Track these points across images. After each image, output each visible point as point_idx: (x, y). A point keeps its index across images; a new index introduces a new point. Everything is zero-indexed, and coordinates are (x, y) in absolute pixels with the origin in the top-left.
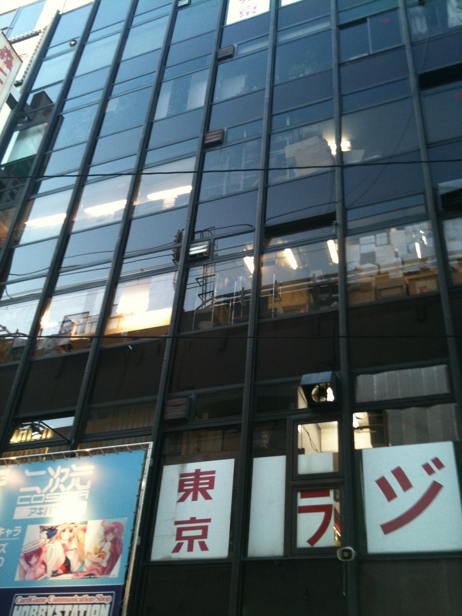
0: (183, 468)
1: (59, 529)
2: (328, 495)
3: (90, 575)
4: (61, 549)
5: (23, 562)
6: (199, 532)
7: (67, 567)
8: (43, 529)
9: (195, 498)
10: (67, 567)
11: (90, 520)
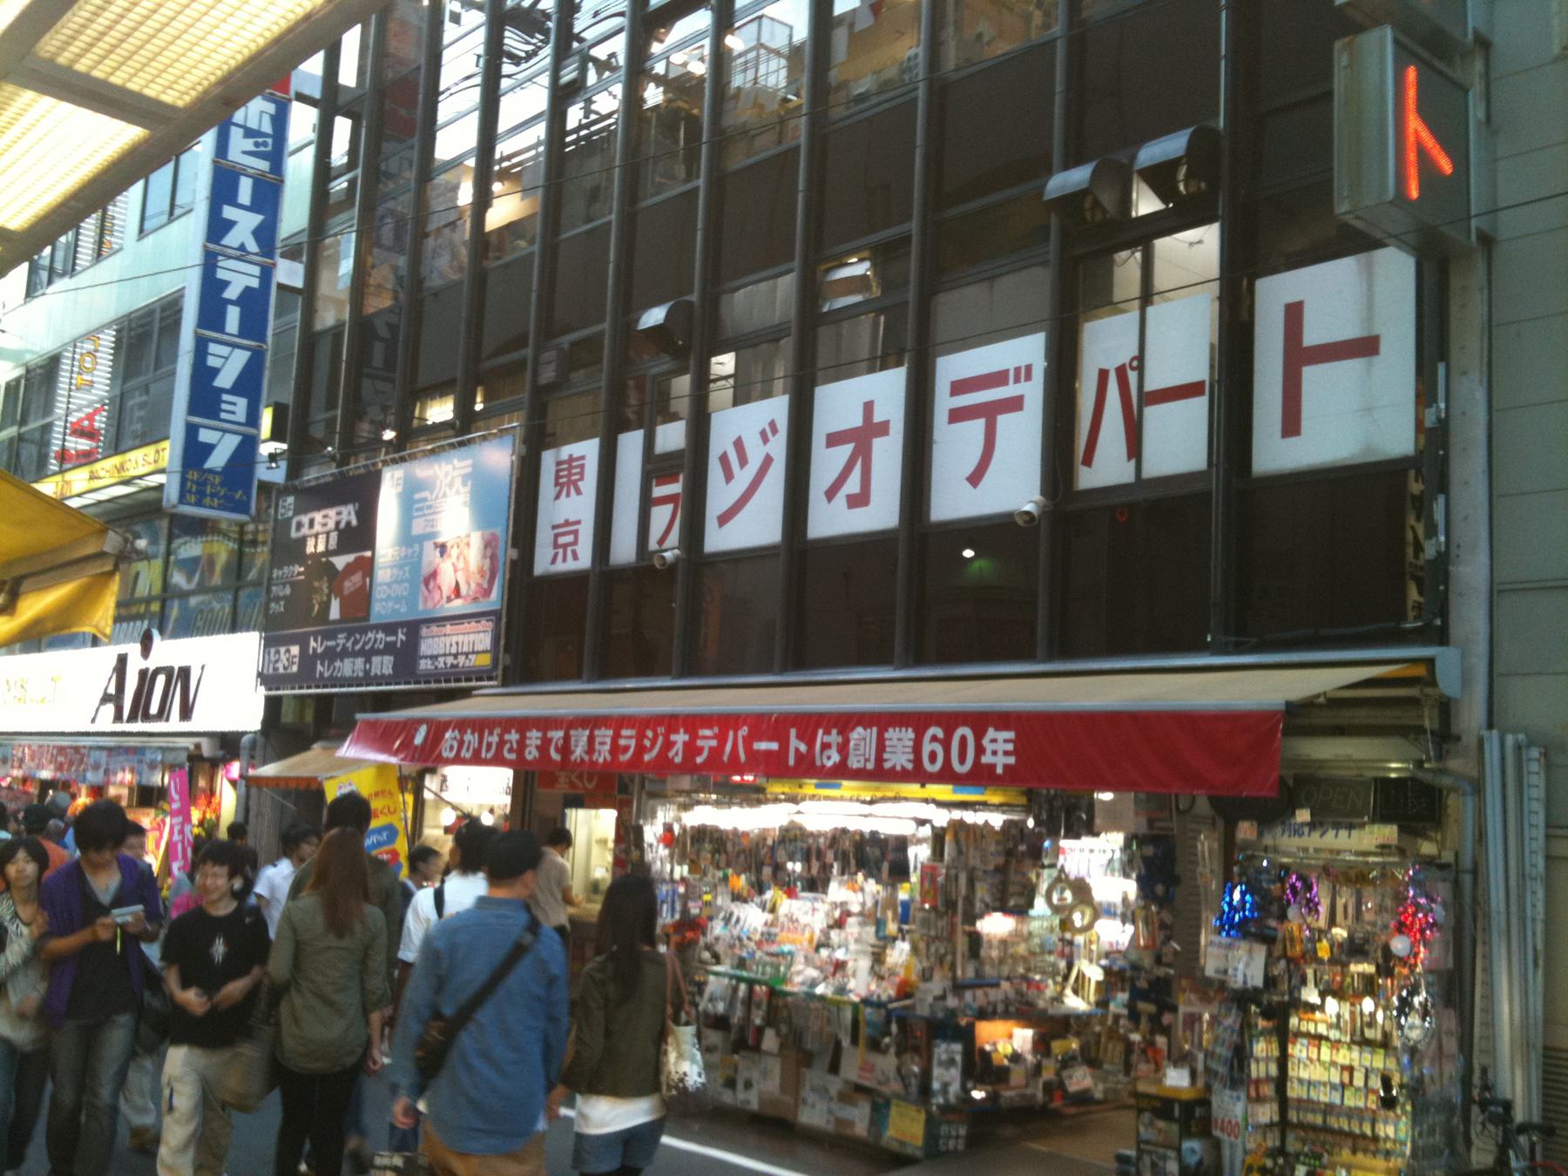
0: (558, 454)
1: (449, 545)
2: (676, 481)
3: (475, 599)
4: (451, 569)
5: (423, 587)
6: (570, 538)
7: (457, 592)
8: (436, 546)
9: (568, 495)
10: (457, 592)
11: (104, 543)
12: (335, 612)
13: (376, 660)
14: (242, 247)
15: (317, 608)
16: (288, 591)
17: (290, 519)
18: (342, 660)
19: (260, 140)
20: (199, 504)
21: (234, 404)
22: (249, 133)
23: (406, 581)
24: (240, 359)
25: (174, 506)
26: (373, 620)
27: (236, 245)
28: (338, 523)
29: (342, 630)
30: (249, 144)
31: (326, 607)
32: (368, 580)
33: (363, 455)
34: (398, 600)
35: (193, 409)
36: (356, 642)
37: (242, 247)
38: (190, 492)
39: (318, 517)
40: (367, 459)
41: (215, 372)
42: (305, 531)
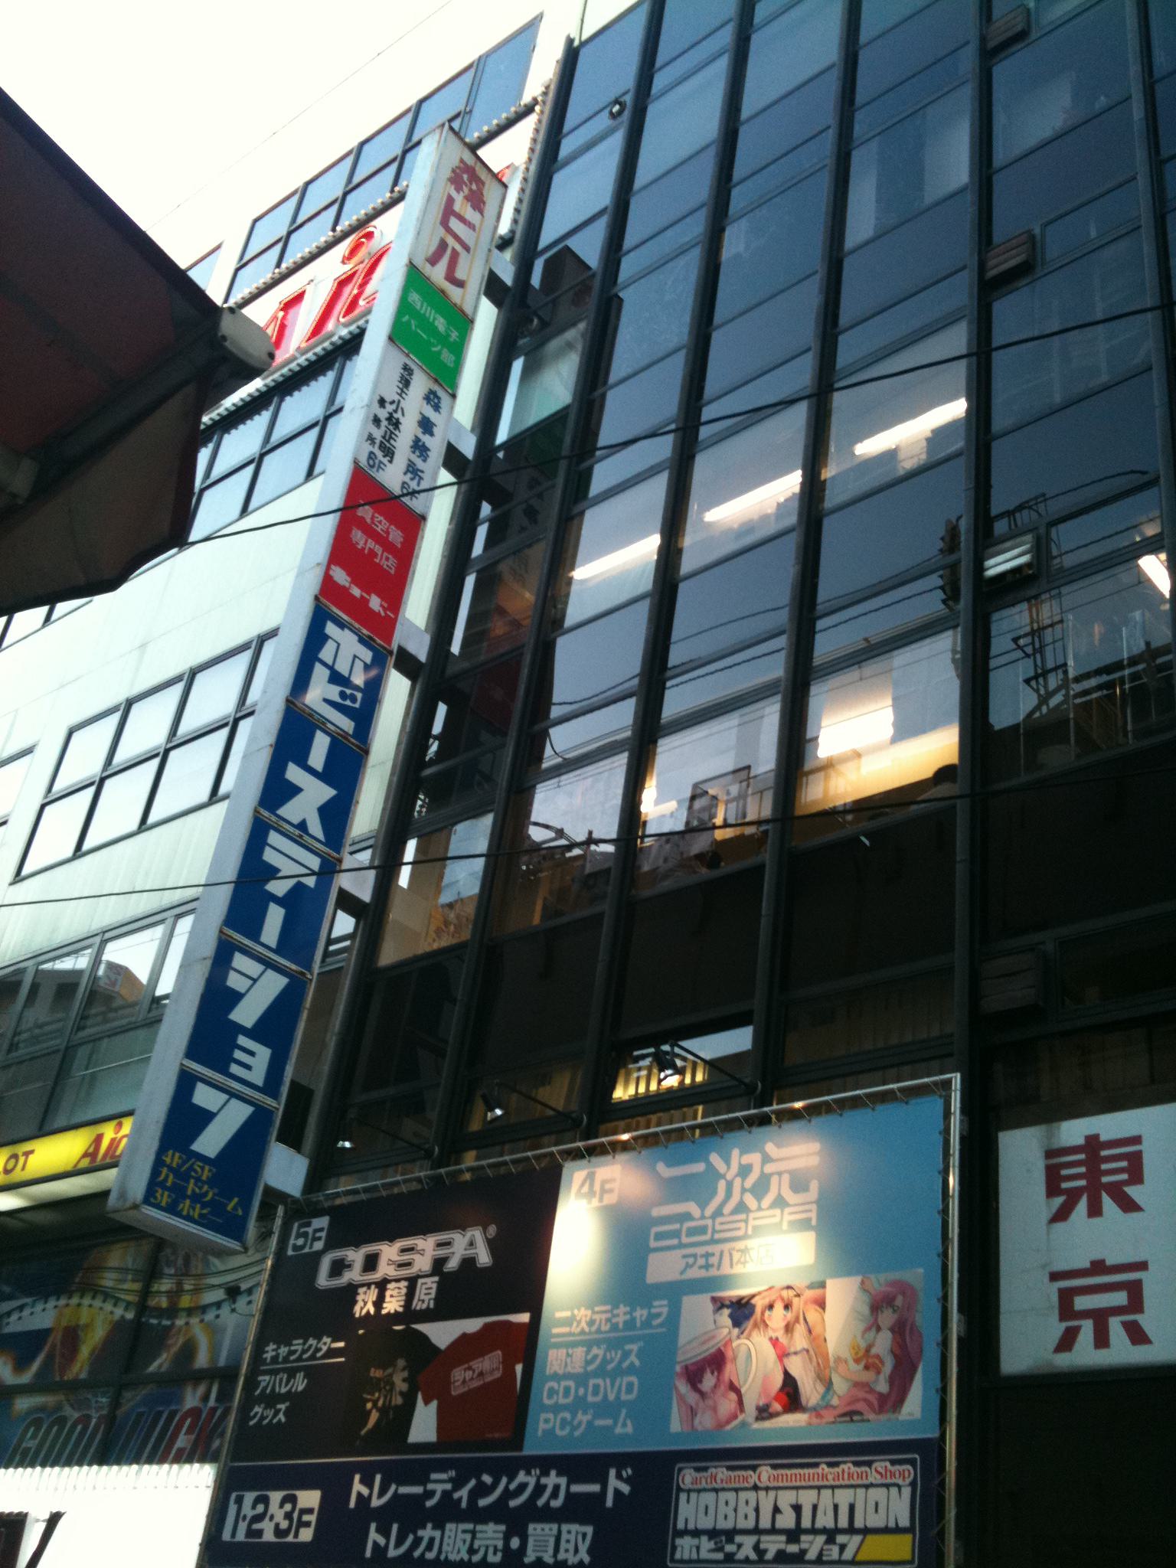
1: (759, 1303)
3: (850, 1415)
4: (770, 1353)
6: (1120, 1298)
7: (790, 1395)
8: (719, 1304)
9: (1095, 1210)
10: (790, 1395)
12: (424, 1425)
13: (540, 1533)
14: (302, 826)
15: (374, 1416)
16: (300, 1384)
17: (318, 1255)
18: (440, 1526)
19: (348, 692)
20: (172, 1209)
21: (252, 1054)
22: (336, 678)
23: (631, 1371)
24: (273, 984)
25: (135, 1207)
26: (529, 1450)
27: (296, 821)
28: (439, 1264)
29: (443, 1467)
30: (334, 692)
31: (404, 1416)
32: (519, 1368)
33: (472, 1154)
34: (607, 1408)
35: (194, 1050)
36: (482, 1490)
37: (302, 826)
38: (162, 1185)
39: (389, 1252)
40: (478, 1158)
41: (236, 997)
42: (354, 1275)
